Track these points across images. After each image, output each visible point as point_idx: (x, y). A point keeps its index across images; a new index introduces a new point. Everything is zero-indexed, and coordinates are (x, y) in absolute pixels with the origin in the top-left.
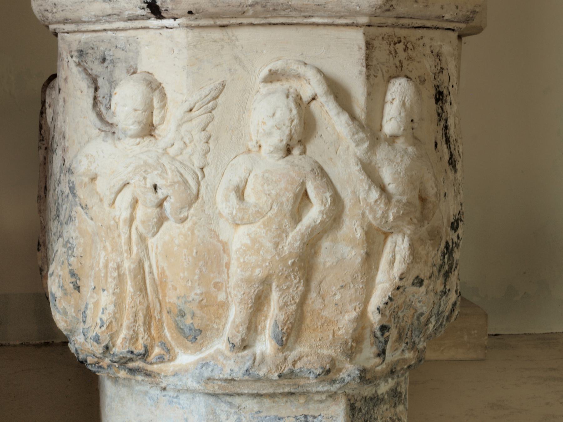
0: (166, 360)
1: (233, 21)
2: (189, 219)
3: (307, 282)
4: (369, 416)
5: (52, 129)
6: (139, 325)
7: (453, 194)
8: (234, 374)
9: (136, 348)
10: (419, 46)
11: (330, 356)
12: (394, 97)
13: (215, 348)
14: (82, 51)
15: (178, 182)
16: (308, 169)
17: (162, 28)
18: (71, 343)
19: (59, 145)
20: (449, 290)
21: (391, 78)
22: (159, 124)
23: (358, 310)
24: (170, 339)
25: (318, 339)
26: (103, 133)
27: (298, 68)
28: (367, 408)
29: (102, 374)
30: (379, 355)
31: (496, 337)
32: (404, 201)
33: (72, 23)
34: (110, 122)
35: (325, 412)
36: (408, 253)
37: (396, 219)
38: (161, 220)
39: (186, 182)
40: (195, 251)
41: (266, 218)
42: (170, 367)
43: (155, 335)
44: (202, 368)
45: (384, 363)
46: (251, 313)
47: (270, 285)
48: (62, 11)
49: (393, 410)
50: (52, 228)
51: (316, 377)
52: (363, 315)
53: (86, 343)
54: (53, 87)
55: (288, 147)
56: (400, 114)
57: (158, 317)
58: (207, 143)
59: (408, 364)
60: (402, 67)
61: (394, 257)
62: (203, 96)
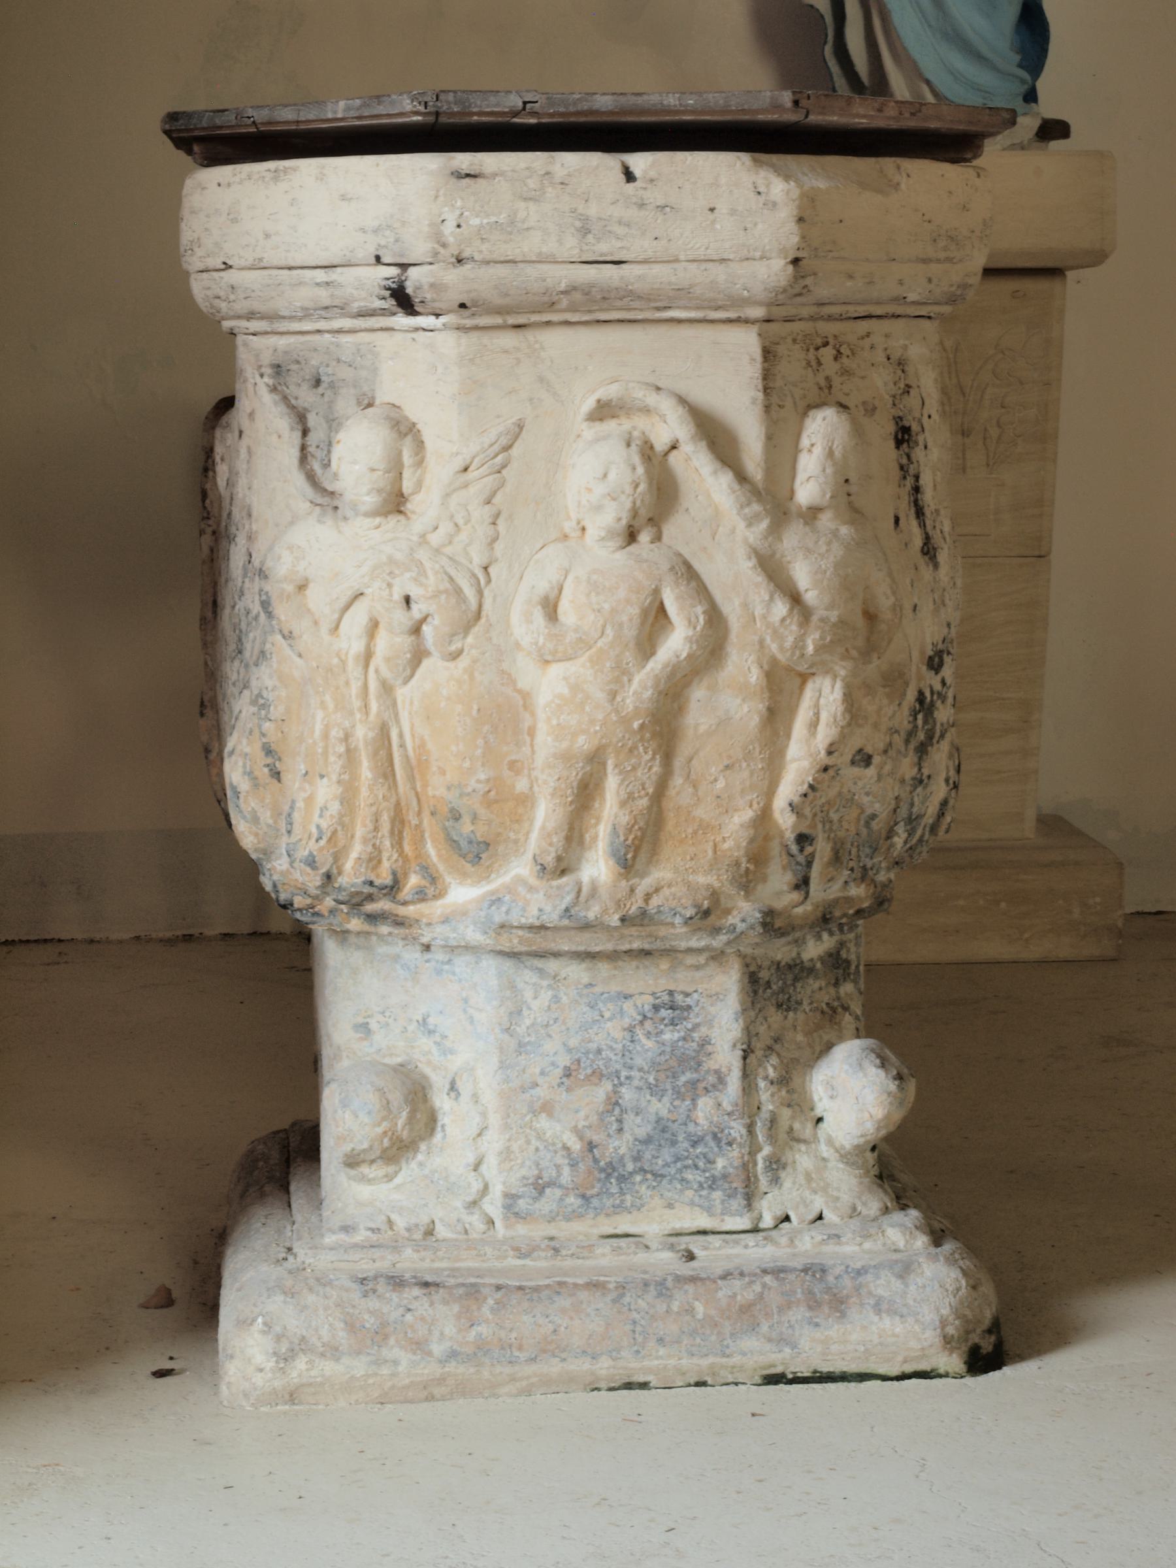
0: (430, 896)
1: (535, 318)
2: (465, 653)
3: (668, 758)
4: (786, 996)
5: (228, 501)
6: (383, 836)
7: (931, 606)
8: (544, 917)
9: (378, 876)
10: (863, 349)
11: (709, 886)
12: (814, 441)
13: (513, 873)
14: (279, 366)
15: (446, 591)
16: (665, 566)
17: (417, 329)
18: (264, 875)
19: (240, 527)
20: (929, 777)
21: (810, 407)
22: (413, 494)
23: (755, 806)
24: (435, 859)
25: (688, 858)
26: (318, 508)
27: (645, 396)
28: (781, 982)
29: (319, 929)
30: (797, 887)
31: (1158, 917)
32: (834, 619)
33: (262, 318)
34: (330, 489)
35: (705, 986)
36: (841, 709)
37: (819, 649)
38: (418, 656)
39: (458, 591)
40: (475, 707)
41: (594, 650)
42: (436, 908)
43: (410, 854)
44: (490, 906)
45: (809, 902)
46: (572, 812)
47: (604, 764)
48: (246, 298)
49: (832, 990)
50: (229, 673)
51: (686, 923)
52: (764, 816)
53: (292, 870)
54: (228, 425)
55: (631, 529)
56: (824, 470)
57: (414, 822)
58: (494, 524)
59: (857, 908)
60: (830, 387)
61: (817, 715)
62: (486, 446)
